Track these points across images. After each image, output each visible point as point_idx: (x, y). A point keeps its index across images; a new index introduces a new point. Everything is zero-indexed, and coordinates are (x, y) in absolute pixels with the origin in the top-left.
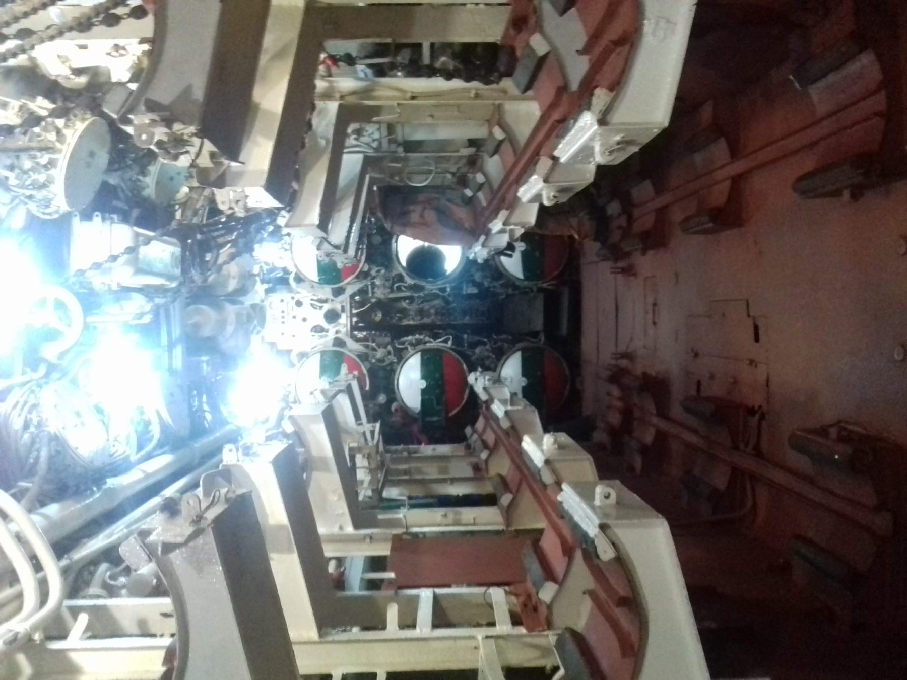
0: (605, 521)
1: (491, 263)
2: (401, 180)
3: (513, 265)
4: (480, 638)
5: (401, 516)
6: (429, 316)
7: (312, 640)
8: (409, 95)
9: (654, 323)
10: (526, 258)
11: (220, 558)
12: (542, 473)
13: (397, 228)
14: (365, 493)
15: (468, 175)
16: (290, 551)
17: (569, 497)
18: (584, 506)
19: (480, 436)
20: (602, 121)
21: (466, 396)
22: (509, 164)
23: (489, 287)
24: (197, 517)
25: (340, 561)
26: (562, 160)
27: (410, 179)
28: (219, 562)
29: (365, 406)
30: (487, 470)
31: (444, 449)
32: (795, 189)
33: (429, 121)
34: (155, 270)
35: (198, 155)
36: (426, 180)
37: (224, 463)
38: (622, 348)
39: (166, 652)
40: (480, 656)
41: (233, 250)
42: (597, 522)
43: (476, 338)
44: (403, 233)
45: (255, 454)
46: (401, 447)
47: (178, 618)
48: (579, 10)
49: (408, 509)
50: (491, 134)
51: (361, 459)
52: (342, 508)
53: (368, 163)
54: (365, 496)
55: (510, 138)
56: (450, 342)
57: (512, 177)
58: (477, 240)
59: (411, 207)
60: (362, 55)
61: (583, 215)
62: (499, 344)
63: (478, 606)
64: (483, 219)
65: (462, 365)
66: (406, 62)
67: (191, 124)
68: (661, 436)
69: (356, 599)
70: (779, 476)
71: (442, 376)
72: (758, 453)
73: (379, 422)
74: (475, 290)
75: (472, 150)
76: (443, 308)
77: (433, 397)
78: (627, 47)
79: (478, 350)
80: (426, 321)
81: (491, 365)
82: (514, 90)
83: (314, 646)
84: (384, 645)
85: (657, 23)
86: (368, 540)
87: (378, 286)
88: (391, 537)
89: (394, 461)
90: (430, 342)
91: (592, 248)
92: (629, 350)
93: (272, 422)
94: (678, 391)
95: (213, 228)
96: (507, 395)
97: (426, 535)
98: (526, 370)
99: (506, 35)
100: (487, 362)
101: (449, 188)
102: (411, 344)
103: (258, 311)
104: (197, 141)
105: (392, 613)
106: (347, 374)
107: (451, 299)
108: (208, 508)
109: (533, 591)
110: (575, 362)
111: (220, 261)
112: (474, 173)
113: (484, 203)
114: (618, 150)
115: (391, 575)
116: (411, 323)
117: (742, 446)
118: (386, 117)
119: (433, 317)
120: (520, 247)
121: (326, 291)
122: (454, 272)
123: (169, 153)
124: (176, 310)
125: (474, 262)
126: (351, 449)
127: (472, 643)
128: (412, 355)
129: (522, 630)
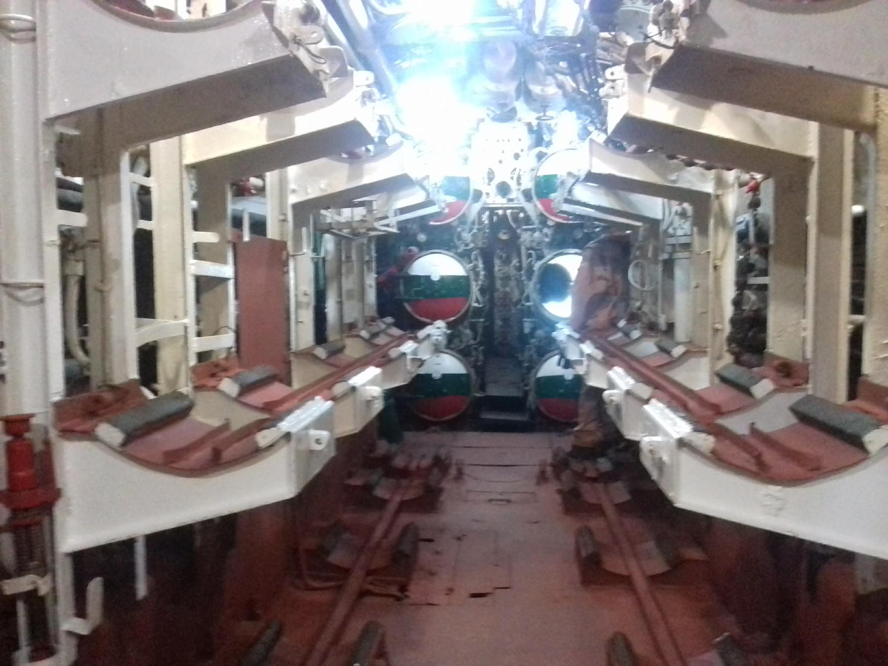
0: (294, 439)
1: (553, 347)
2: (636, 258)
3: (550, 368)
4: (186, 321)
5: (305, 250)
6: (504, 285)
7: (183, 158)
8: (718, 263)
9: (491, 501)
10: (555, 381)
11: (261, 63)
12: (344, 383)
13: (588, 253)
14: (329, 216)
15: (639, 323)
16: (269, 137)
17: (319, 406)
18: (310, 420)
19: (383, 331)
20: (682, 443)
21: (423, 319)
22: (645, 361)
23: (528, 344)
24: (300, 40)
25: (261, 191)
26: (646, 407)
27: (636, 265)
28: (255, 62)
29: (413, 220)
30: (348, 337)
31: (371, 296)
32: (616, 634)
33: (693, 284)
34: (550, 9)
35: (658, 44)
36: (636, 282)
37: (355, 73)
38: (467, 470)
39: (171, 11)
40: (167, 320)
41: (569, 88)
42: (293, 430)
43: (480, 331)
44: (584, 260)
45: (364, 103)
46: (374, 254)
47: (202, 20)
48: (793, 425)
49: (313, 259)
50: (678, 344)
51: (361, 214)
52: (313, 193)
53: (654, 224)
54: (324, 216)
55: (674, 363)
56: (476, 305)
57: (635, 364)
58: (575, 330)
59: (609, 268)
60: (758, 217)
61: (599, 436)
62: (474, 353)
63: (217, 320)
64: (595, 337)
65: (453, 316)
66: (751, 261)
67: (688, 36)
68: (382, 504)
69: (225, 209)
70: (340, 612)
71: (444, 296)
72: (363, 594)
73: (398, 232)
74: (527, 330)
75: (663, 326)
76: (511, 300)
77: (422, 287)
78: (754, 468)
79: (468, 332)
80: (498, 284)
81: (452, 344)
82: (720, 365)
83: (177, 159)
84: (179, 228)
85: (778, 499)
86: (282, 217)
87: (532, 235)
88: (285, 239)
89: (360, 247)
90: (477, 285)
91: (565, 443)
92: (465, 477)
93: (399, 127)
94: (424, 521)
95: (592, 69)
96: (425, 356)
97: (286, 275)
98: (449, 379)
99: (774, 357)
100: (456, 341)
101: (628, 306)
102: (475, 267)
103: (507, 115)
104: (671, 43)
105: (209, 237)
106: (445, 201)
107: (519, 307)
108: (309, 51)
109: (231, 373)
110: (455, 425)
111: (560, 77)
112: (642, 328)
113: (611, 338)
114: (653, 459)
115: (246, 238)
116: (496, 268)
117: (369, 578)
118: (697, 241)
119: (502, 290)
120: (569, 374)
121: (528, 183)
122: (545, 309)
123: (660, 14)
124: (511, 32)
125: (554, 329)
126: (371, 202)
127: (180, 313)
128: (464, 267)
129: (193, 361)
